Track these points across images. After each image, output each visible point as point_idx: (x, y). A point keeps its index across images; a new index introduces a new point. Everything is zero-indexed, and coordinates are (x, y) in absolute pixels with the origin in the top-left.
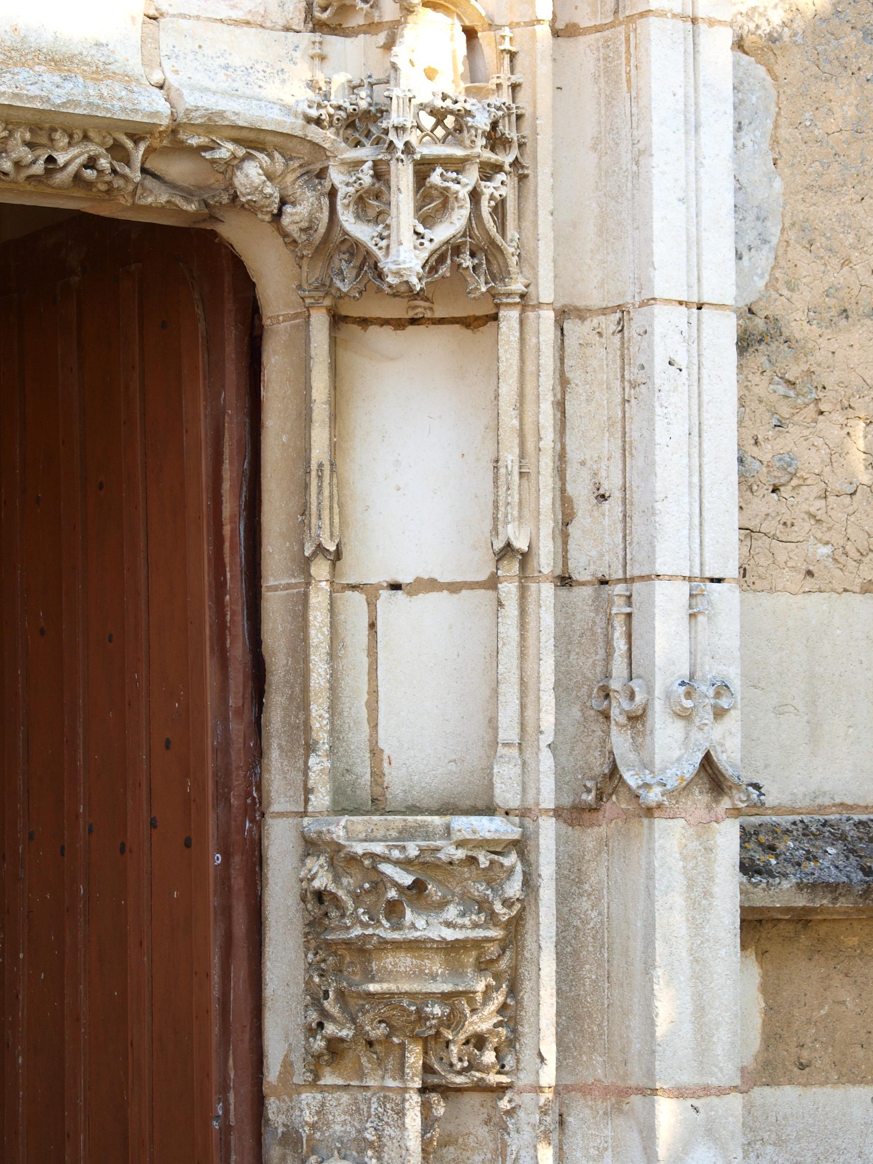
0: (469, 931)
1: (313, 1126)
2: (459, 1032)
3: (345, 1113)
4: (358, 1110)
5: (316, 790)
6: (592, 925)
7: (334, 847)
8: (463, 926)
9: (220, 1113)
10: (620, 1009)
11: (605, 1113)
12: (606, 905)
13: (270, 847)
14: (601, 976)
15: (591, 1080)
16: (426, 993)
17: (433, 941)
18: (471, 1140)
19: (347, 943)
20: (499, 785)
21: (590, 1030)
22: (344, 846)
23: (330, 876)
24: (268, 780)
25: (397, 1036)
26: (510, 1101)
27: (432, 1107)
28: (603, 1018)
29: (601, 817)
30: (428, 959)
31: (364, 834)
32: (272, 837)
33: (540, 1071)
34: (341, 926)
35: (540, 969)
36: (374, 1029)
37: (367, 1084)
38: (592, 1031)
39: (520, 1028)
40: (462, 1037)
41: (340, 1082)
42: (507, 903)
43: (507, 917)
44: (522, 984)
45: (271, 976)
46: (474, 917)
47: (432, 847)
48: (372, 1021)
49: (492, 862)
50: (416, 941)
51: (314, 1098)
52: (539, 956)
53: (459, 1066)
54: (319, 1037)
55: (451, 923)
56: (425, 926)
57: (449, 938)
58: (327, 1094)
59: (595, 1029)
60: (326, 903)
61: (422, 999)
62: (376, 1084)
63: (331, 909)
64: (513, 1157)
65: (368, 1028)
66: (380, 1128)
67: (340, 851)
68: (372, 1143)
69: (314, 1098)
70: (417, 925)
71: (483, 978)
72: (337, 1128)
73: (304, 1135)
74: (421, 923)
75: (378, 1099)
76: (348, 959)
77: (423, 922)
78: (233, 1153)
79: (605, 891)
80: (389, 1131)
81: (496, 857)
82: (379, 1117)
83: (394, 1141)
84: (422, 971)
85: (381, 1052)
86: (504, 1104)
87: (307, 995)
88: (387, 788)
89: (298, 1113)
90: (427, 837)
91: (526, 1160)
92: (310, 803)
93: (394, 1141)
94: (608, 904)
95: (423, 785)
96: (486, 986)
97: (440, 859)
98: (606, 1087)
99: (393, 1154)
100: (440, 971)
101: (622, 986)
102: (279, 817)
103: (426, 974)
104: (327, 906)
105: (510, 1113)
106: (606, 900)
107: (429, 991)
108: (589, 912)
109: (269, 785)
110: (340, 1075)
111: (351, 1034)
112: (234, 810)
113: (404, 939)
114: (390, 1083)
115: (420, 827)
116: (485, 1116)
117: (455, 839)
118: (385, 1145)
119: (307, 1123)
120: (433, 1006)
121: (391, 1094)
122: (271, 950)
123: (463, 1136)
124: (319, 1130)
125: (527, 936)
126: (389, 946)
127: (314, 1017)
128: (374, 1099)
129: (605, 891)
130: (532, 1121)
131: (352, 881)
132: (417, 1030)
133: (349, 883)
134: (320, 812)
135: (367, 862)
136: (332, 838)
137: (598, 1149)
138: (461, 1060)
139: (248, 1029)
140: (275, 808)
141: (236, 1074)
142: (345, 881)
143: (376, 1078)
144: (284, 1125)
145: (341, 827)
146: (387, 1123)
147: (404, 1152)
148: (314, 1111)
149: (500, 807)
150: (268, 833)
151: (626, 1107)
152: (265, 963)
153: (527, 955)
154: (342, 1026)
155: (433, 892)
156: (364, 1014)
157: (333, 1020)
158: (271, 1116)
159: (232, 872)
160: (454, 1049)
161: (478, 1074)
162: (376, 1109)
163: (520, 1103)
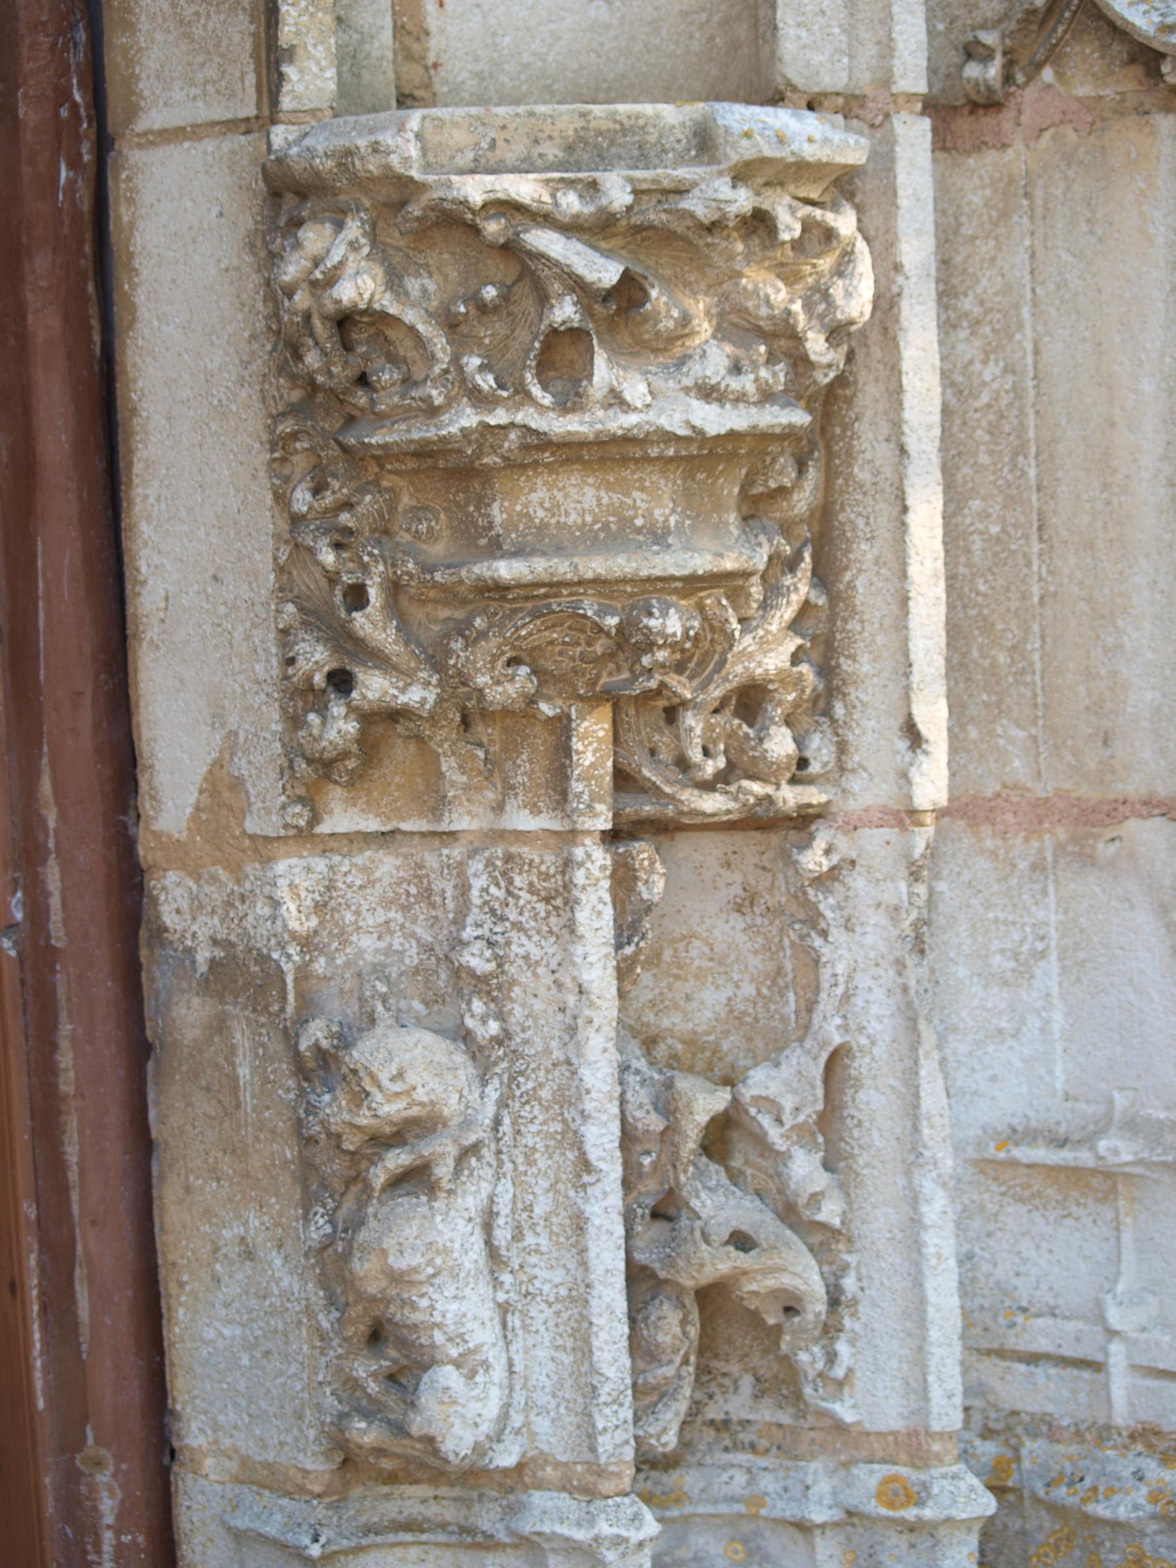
0: (754, 410)
1: (307, 943)
2: (709, 681)
3: (387, 904)
4: (426, 894)
5: (300, 51)
6: (984, 399)
7: (386, 193)
8: (740, 398)
9: (19, 916)
10: (1082, 606)
11: (1037, 867)
12: (1029, 347)
13: (141, 224)
14: (1016, 526)
15: (991, 787)
16: (649, 580)
17: (669, 437)
18: (694, 953)
19: (425, 452)
20: (792, 32)
21: (987, 663)
22: (423, 187)
23: (379, 271)
24: (125, 50)
25: (549, 699)
26: (827, 852)
27: (636, 879)
28: (1027, 630)
29: (1007, 126)
30: (642, 489)
31: (470, 155)
32: (147, 196)
33: (913, 773)
34: (409, 408)
35: (905, 509)
36: (498, 683)
37: (453, 828)
38: (994, 665)
39: (846, 665)
40: (716, 692)
41: (373, 824)
42: (837, 332)
43: (832, 375)
44: (848, 551)
45: (156, 560)
46: (764, 373)
47: (666, 184)
48: (494, 658)
49: (808, 226)
50: (627, 439)
51: (309, 870)
52: (901, 477)
53: (711, 767)
54: (337, 709)
55: (714, 388)
56: (649, 399)
57: (712, 430)
58: (337, 858)
59: (1002, 658)
60: (362, 349)
61: (632, 595)
62: (475, 825)
63: (376, 366)
64: (839, 991)
65: (482, 680)
66: (499, 938)
67: (403, 204)
68: (483, 979)
69: (309, 870)
70: (627, 396)
71: (762, 538)
72: (367, 942)
73: (287, 967)
74: (636, 390)
75: (489, 863)
76: (406, 501)
77: (642, 388)
78: (63, 1016)
79: (1026, 312)
80: (522, 945)
81: (818, 213)
82: (493, 911)
83: (541, 970)
84: (626, 523)
85: (491, 741)
86: (814, 860)
87: (282, 601)
88: (435, 66)
89: (262, 909)
90: (642, 157)
91: (871, 997)
92: (286, 88)
93: (541, 970)
94: (1036, 343)
95: (526, 58)
96: (770, 558)
97: (690, 215)
98: (1037, 804)
99: (538, 1005)
100: (672, 520)
101: (1091, 545)
102: (169, 141)
103: (639, 531)
104: (366, 358)
105: (828, 879)
106: (1029, 333)
107: (657, 572)
108: (977, 367)
109: (130, 63)
110: (371, 807)
111: (431, 696)
112: (28, 136)
113: (598, 433)
114: (522, 820)
115: (624, 131)
116: (737, 890)
117: (734, 158)
118: (514, 982)
119: (294, 936)
120: (665, 614)
121: (525, 851)
122: (152, 492)
123: (672, 942)
124: (321, 952)
125: (861, 427)
126: (547, 457)
127: (317, 657)
128: (477, 865)
129: (1026, 312)
130: (888, 898)
131: (431, 287)
132: (604, 679)
133: (424, 290)
134: (313, 112)
135: (493, 228)
136: (388, 167)
137: (1016, 956)
138: (706, 752)
139: (87, 700)
140: (153, 119)
141: (62, 816)
142: (413, 285)
143: (474, 810)
144: (215, 942)
145: (411, 135)
146: (518, 926)
147: (571, 999)
148: (309, 902)
149: (794, 89)
150: (133, 190)
151: (1105, 851)
152: (131, 527)
153: (862, 474)
154: (407, 676)
155: (663, 309)
156: (470, 643)
157: (379, 660)
158: (169, 919)
159: (29, 296)
160: (692, 722)
161: (757, 788)
162: (485, 890)
163: (854, 855)
